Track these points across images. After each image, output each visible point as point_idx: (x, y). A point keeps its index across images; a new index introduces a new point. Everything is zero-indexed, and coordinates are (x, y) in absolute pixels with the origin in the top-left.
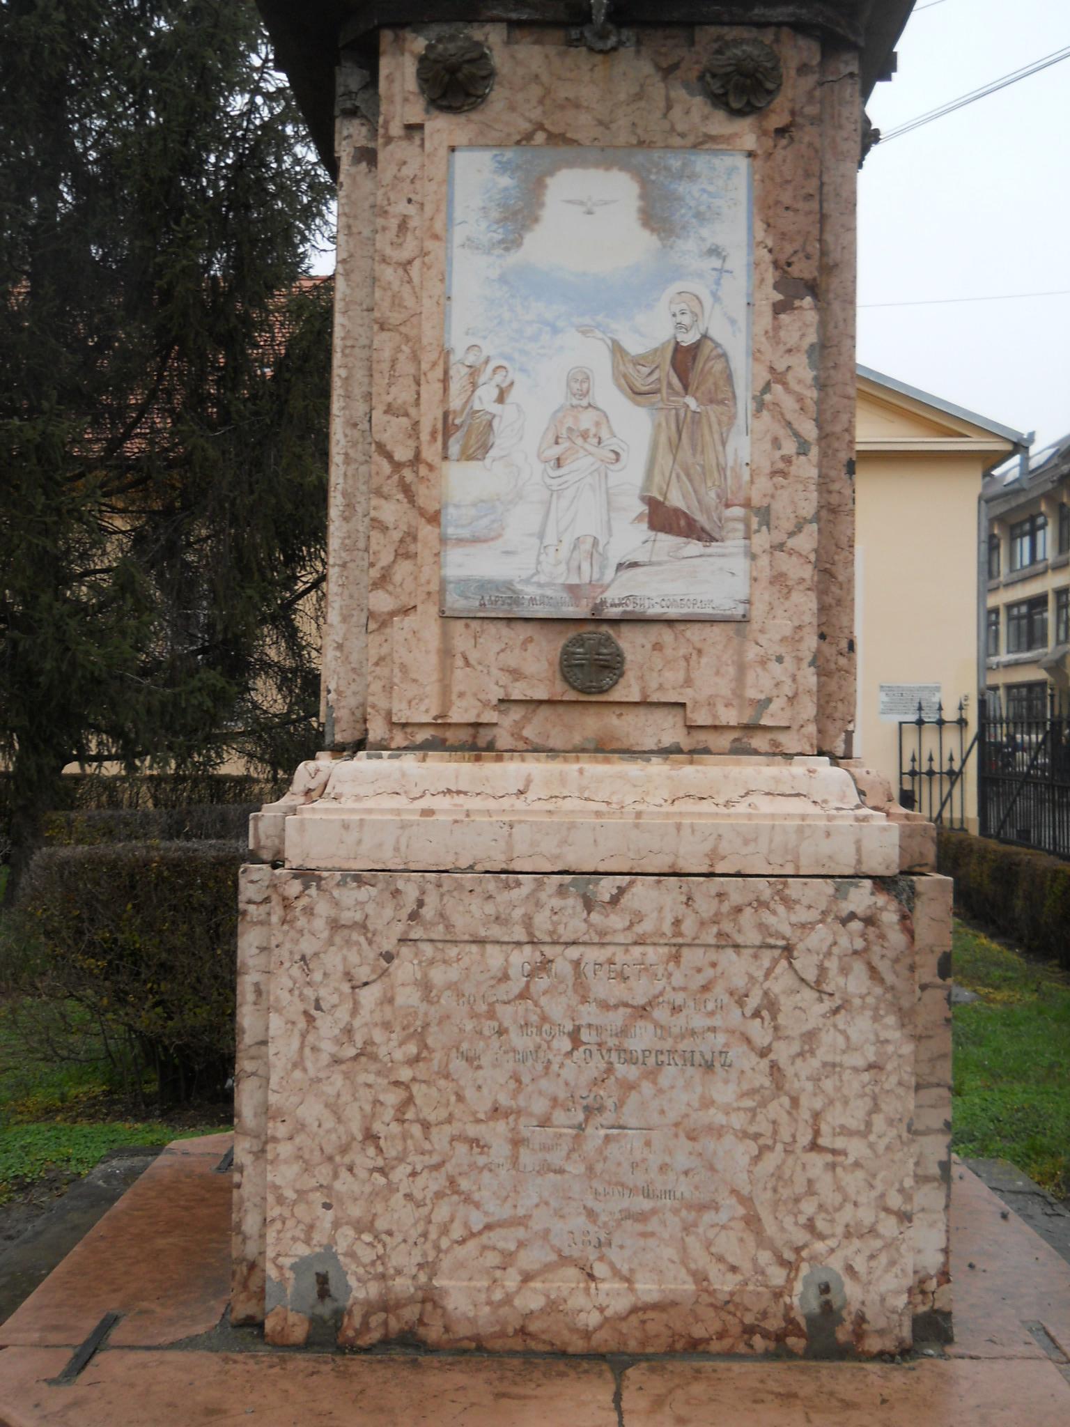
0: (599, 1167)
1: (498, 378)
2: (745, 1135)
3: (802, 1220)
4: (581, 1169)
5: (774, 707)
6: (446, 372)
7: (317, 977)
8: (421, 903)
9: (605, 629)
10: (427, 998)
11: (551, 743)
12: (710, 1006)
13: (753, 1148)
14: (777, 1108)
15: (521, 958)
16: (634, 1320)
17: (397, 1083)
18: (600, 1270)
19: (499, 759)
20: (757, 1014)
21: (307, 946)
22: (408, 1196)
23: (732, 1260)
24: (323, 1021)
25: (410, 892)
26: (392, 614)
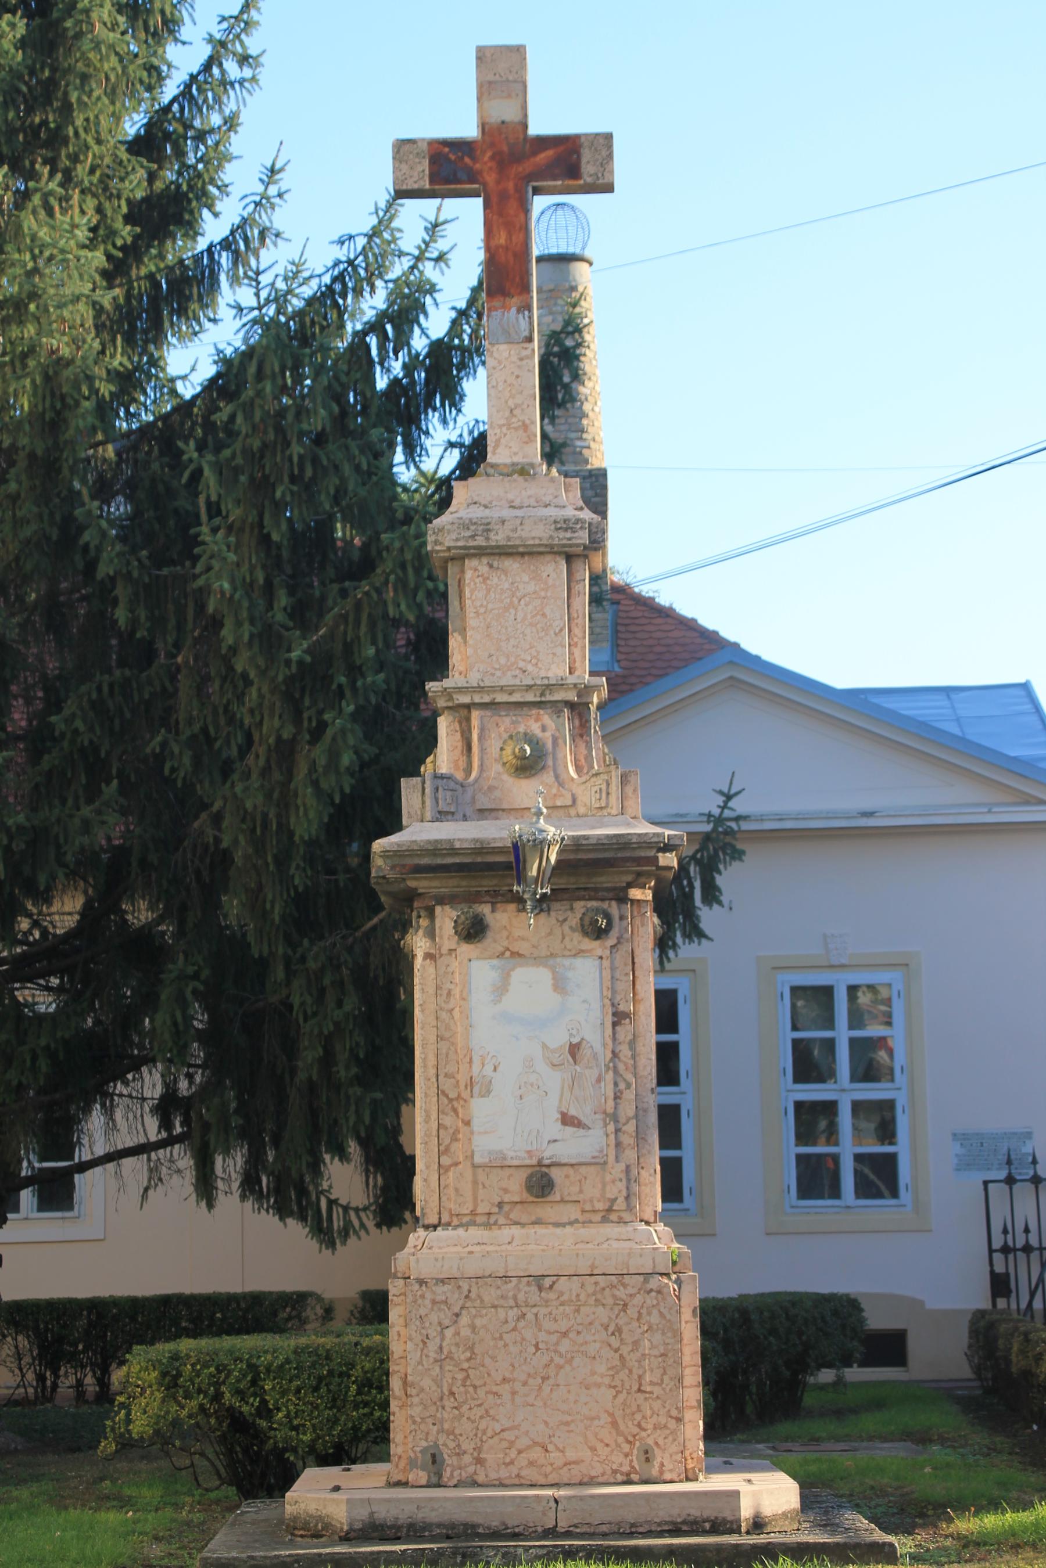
0: (549, 1403)
1: (494, 1060)
2: (610, 1386)
3: (636, 1422)
4: (541, 1404)
5: (618, 1201)
6: (471, 1059)
7: (427, 1324)
8: (470, 1291)
9: (544, 1169)
10: (473, 1332)
11: (522, 1221)
12: (593, 1331)
13: (613, 1392)
14: (623, 1375)
15: (513, 1313)
16: (565, 1469)
17: (462, 1370)
18: (550, 1447)
19: (500, 1229)
20: (613, 1334)
21: (422, 1312)
22: (468, 1418)
23: (606, 1441)
25: (465, 1287)
26: (451, 1166)
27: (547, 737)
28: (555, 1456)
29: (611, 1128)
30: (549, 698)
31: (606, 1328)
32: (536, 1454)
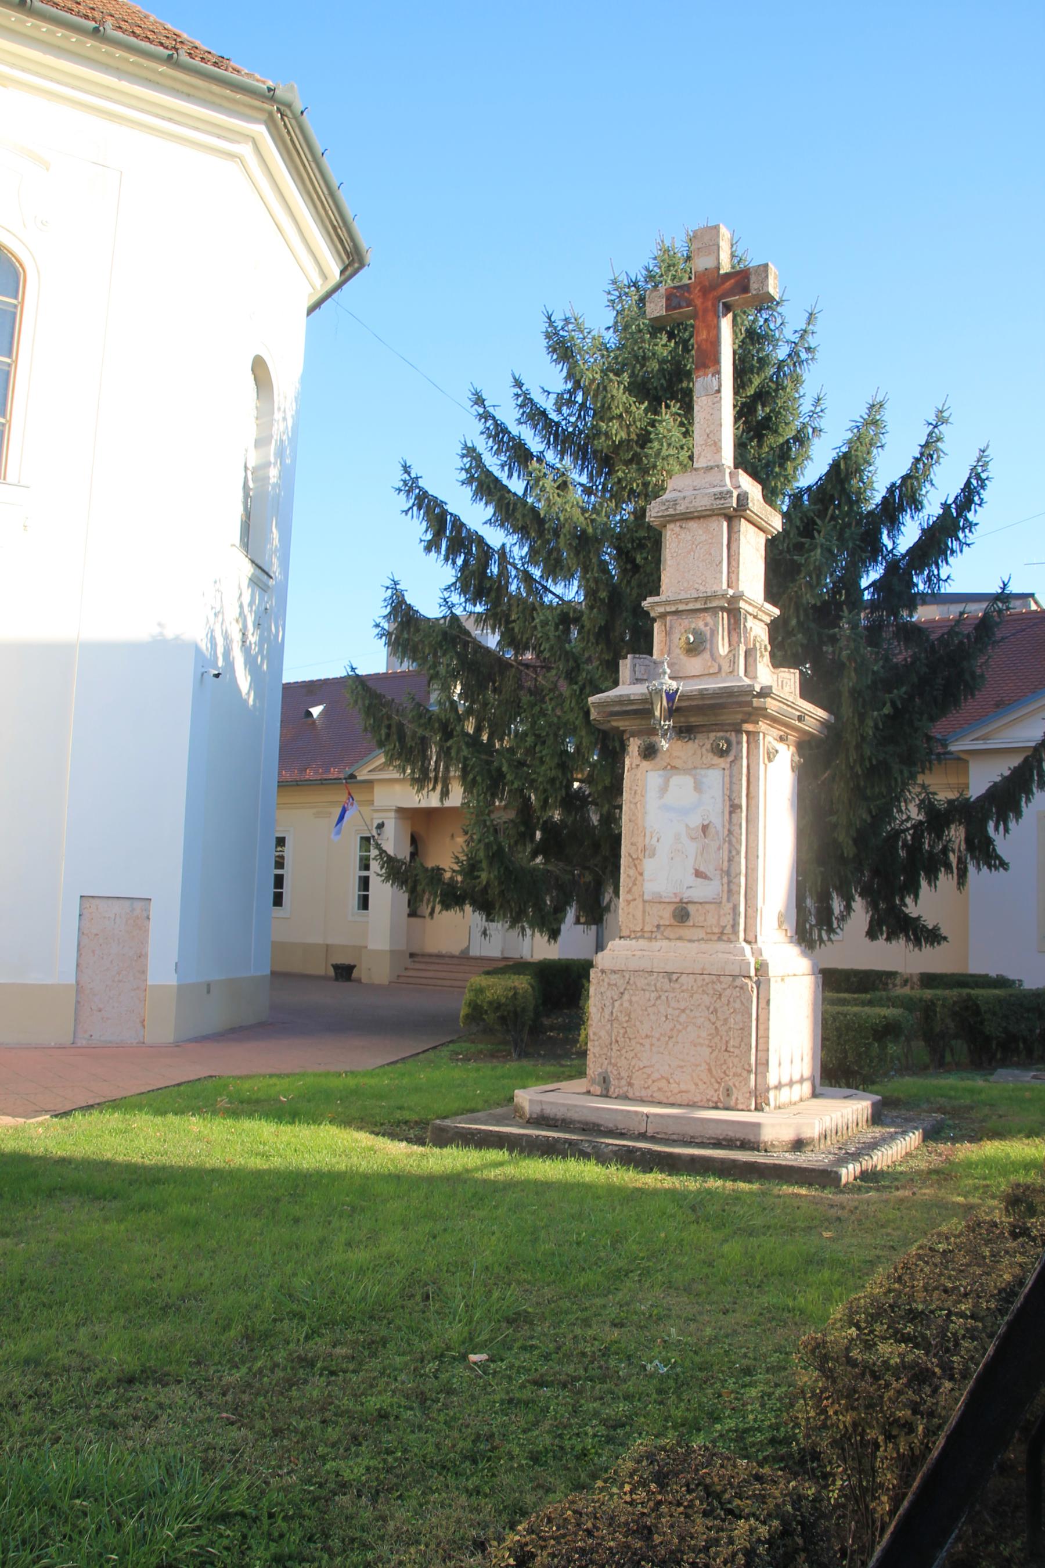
14: (717, 1039)
15: (654, 995)
18: (671, 1081)
21: (602, 990)
24: (606, 1010)
25: (627, 976)
27: (707, 631)
28: (673, 1086)
29: (725, 880)
30: (709, 605)
31: (708, 1009)
32: (663, 1084)
